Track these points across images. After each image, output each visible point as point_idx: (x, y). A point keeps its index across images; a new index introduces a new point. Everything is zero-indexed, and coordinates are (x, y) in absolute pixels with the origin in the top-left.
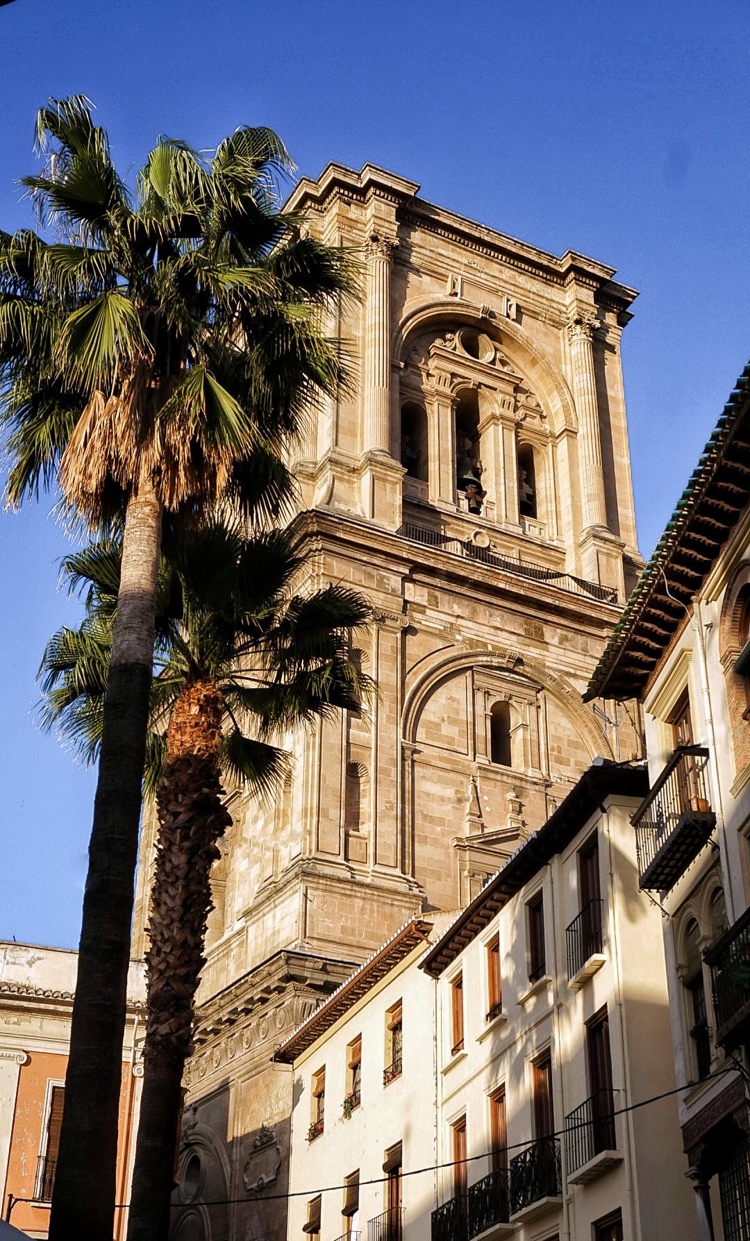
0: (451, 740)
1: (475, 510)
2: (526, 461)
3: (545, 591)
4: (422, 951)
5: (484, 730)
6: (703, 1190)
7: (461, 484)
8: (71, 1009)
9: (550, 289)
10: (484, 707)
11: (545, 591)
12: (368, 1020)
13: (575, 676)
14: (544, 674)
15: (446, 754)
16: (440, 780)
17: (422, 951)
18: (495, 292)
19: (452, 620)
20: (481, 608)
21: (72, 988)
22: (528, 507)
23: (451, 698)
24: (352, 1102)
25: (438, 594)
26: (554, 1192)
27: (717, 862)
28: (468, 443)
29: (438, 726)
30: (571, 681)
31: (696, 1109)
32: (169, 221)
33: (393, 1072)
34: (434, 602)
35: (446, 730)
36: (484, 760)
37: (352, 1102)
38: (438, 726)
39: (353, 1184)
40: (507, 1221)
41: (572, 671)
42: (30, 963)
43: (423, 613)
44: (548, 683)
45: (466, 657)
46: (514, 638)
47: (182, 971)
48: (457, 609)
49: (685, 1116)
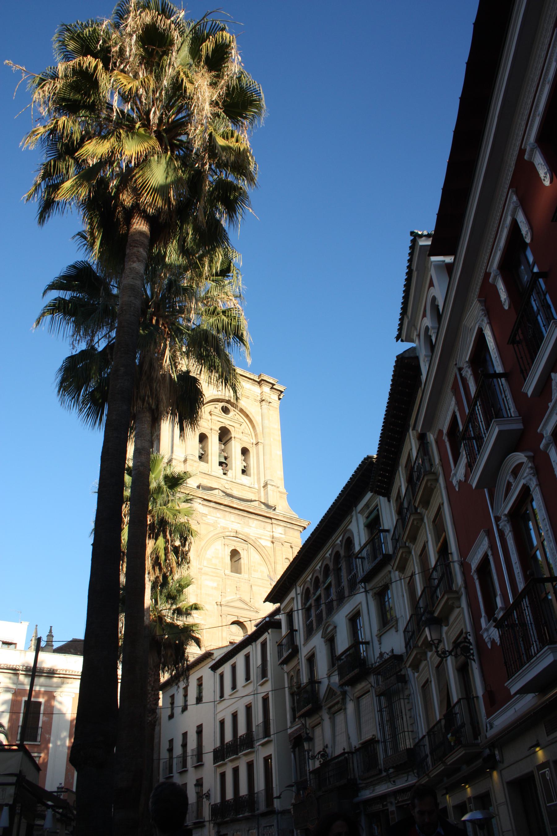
3: (250, 507)
6: (294, 752)
8: (80, 677)
9: (253, 387)
11: (250, 507)
13: (260, 538)
19: (216, 519)
20: (227, 514)
21: (80, 669)
26: (252, 747)
27: (299, 663)
30: (259, 540)
33: (199, 700)
36: (228, 572)
37: (185, 708)
40: (237, 754)
41: (260, 537)
43: (206, 517)
45: (221, 533)
46: (239, 525)
47: (154, 702)
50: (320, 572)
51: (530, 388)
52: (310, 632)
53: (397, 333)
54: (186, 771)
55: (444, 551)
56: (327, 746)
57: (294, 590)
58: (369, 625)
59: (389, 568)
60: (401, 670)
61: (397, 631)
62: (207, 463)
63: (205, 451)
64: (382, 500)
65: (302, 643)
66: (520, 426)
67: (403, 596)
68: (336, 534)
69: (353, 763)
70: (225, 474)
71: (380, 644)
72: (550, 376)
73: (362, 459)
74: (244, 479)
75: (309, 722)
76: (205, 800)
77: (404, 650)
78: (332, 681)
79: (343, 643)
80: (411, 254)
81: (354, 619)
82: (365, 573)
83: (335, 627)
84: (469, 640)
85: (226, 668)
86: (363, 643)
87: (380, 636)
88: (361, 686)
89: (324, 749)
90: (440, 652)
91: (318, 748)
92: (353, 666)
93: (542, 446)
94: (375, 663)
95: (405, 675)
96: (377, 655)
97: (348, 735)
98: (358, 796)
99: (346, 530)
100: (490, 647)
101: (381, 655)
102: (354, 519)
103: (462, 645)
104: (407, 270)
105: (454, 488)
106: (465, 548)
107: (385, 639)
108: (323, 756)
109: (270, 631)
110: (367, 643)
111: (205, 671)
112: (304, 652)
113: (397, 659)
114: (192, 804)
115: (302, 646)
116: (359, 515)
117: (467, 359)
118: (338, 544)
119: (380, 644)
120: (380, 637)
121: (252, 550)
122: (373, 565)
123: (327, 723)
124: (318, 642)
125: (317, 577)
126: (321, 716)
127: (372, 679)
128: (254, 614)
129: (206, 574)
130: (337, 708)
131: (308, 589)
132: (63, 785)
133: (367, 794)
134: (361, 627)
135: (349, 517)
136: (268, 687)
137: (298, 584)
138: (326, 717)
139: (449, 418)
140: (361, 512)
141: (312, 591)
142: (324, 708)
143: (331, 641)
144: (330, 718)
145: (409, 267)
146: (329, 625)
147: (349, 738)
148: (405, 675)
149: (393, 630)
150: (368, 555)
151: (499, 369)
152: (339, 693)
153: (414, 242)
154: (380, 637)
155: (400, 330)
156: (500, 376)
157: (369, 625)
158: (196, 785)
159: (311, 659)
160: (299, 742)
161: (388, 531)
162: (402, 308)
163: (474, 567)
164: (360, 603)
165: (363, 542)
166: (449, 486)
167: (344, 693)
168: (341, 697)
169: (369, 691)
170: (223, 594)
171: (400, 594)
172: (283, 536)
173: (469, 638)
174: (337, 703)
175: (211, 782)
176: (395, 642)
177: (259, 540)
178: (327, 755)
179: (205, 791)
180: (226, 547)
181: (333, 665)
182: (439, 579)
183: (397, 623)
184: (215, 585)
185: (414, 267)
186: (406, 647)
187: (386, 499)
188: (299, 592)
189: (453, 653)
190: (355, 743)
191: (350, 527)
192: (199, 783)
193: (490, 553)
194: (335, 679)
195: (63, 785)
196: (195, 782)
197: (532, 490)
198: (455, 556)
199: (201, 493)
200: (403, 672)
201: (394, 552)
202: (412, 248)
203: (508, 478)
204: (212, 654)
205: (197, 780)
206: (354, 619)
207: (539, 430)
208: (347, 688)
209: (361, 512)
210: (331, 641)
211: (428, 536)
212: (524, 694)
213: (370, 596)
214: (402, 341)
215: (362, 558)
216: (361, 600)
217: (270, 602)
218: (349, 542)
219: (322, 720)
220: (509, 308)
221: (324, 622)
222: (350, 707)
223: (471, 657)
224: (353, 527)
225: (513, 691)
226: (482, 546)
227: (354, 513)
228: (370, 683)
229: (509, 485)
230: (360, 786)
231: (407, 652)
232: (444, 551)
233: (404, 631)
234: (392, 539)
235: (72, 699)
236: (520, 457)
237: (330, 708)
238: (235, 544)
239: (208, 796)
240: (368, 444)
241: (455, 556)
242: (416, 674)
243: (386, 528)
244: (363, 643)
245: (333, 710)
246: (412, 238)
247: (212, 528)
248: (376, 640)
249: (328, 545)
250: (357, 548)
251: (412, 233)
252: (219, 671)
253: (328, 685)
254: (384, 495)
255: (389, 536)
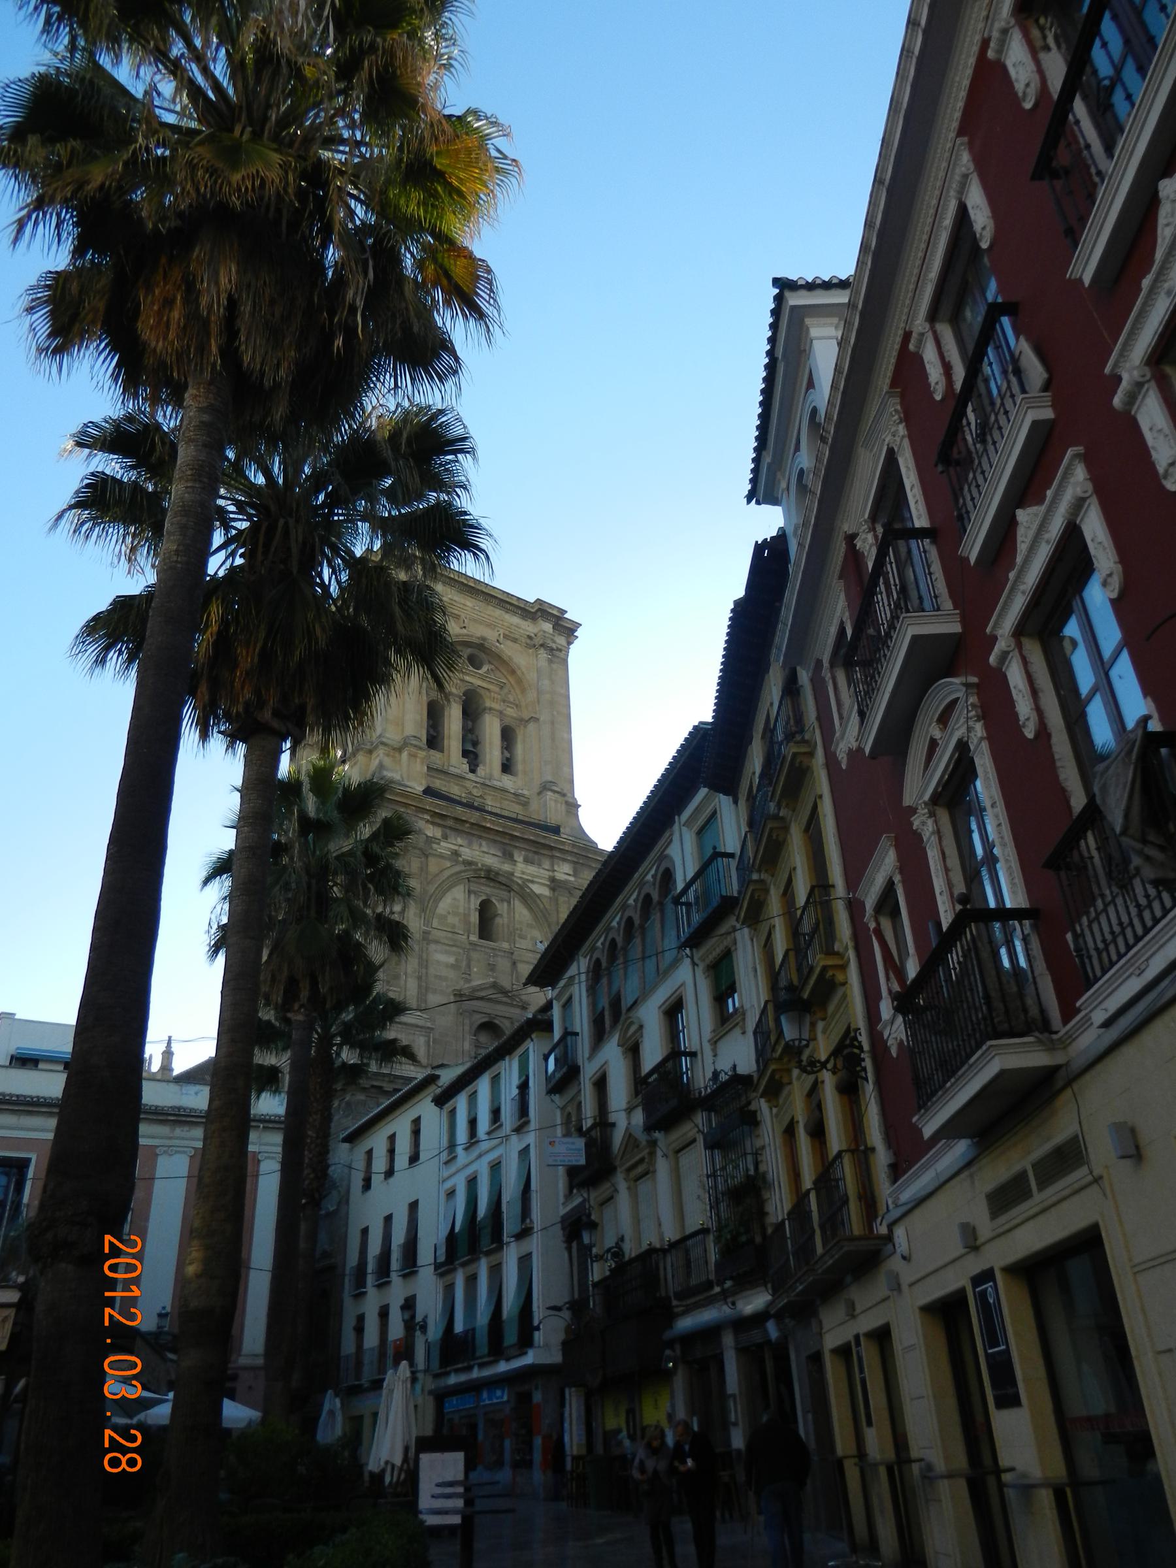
0: (454, 926)
1: (473, 771)
2: (508, 736)
4: (434, 1090)
5: (475, 918)
7: (465, 753)
10: (475, 903)
12: (400, 1125)
13: (532, 882)
14: (513, 881)
15: (450, 935)
16: (447, 952)
17: (434, 1090)
18: (489, 625)
22: (507, 767)
23: (455, 899)
24: (390, 1173)
25: (448, 831)
28: (470, 723)
29: (445, 917)
30: (530, 885)
31: (568, 1208)
32: (384, 1313)
33: (414, 1158)
34: (445, 837)
35: (451, 920)
36: (474, 938)
37: (390, 1173)
38: (445, 917)
39: (388, 1219)
42: (196, 1094)
44: (515, 887)
48: (460, 841)
49: (563, 1211)
50: (618, 930)
51: (973, 548)
52: (599, 1036)
53: (749, 487)
54: (389, 1283)
55: (821, 886)
56: (622, 1239)
57: (575, 964)
58: (698, 1021)
59: (732, 921)
60: (749, 1103)
61: (744, 1033)
62: (442, 751)
63: (438, 732)
64: (724, 802)
65: (587, 1055)
66: (956, 628)
67: (756, 971)
68: (646, 864)
69: (665, 1269)
70: (473, 771)
71: (715, 1056)
72: (1014, 516)
73: (690, 729)
74: (507, 782)
75: (595, 1196)
76: (418, 1333)
77: (754, 1067)
78: (634, 1122)
79: (653, 1053)
80: (774, 327)
81: (673, 1011)
82: (692, 930)
83: (641, 1027)
84: (860, 1043)
85: (461, 1103)
86: (686, 1054)
87: (716, 1042)
88: (687, 1130)
89: (617, 1243)
90: (804, 1063)
91: (610, 1242)
92: (667, 1096)
93: (992, 659)
94: (706, 1088)
95: (755, 1112)
96: (709, 1075)
97: (659, 1218)
98: (671, 1327)
99: (663, 857)
100: (895, 1055)
101: (716, 1074)
102: (676, 837)
103: (846, 1052)
104: (767, 360)
105: (839, 763)
106: (855, 874)
107: (723, 1046)
108: (615, 1255)
109: (533, 1036)
110: (693, 1055)
111: (425, 1108)
112: (589, 1071)
113: (739, 1082)
114: (372, 1349)
115: (586, 1062)
116: (684, 829)
117: (866, 516)
118: (648, 882)
119: (715, 1056)
120: (714, 1043)
121: (518, 905)
122: (705, 915)
123: (623, 1199)
124: (612, 1054)
125: (613, 940)
126: (613, 1185)
127: (700, 1118)
128: (518, 1011)
129: (437, 942)
130: (642, 1172)
131: (598, 962)
132: (168, 1309)
133: (685, 1323)
134: (684, 1027)
135: (667, 834)
136: (531, 1138)
137: (581, 953)
138: (622, 1186)
139: (834, 630)
140: (688, 823)
141: (604, 964)
142: (619, 1170)
143: (633, 1050)
144: (629, 1188)
145: (770, 354)
146: (632, 1023)
147: (660, 1225)
148: (755, 1112)
149: (737, 1031)
150: (697, 898)
151: (920, 519)
152: (644, 1143)
153: (779, 299)
154: (714, 1043)
155: (754, 481)
156: (921, 533)
157: (698, 1021)
158: (403, 1308)
159: (601, 1084)
160: (576, 1227)
161: (732, 855)
162: (757, 438)
163: (870, 903)
164: (683, 984)
165: (690, 874)
166: (831, 761)
167: (653, 1144)
168: (647, 1151)
169: (694, 1141)
170: (467, 975)
171: (750, 965)
172: (572, 879)
173: (860, 1038)
174: (642, 1160)
175: (430, 1304)
176: (740, 1054)
177: (530, 885)
178: (623, 1255)
179: (419, 1318)
180: (472, 896)
181: (637, 1093)
182: (813, 932)
183: (744, 1019)
184: (452, 960)
185: (779, 353)
186: (757, 1062)
187: (731, 798)
188: (583, 970)
189: (829, 1066)
190: (671, 1233)
191: (669, 851)
192: (409, 1305)
193: (897, 879)
194: (639, 1117)
195: (168, 1309)
196: (402, 1302)
197: (972, 748)
198: (840, 889)
199: (430, 803)
200: (753, 1107)
201: (739, 892)
202: (776, 313)
203: (931, 729)
204: (438, 1077)
205: (407, 1300)
206: (673, 1011)
207: (988, 630)
208: (657, 1135)
209: (688, 823)
210: (633, 1050)
211: (797, 856)
212: (954, 1138)
213: (699, 971)
214: (758, 503)
215: (688, 905)
216: (688, 979)
217: (535, 984)
218: (668, 876)
219: (616, 1191)
220: (943, 399)
221: (623, 1018)
222: (662, 1167)
223: (863, 1074)
224: (674, 851)
225: (928, 1131)
226: (886, 865)
227: (676, 827)
228: (697, 1126)
229: (933, 744)
230: (676, 1310)
231: (758, 1070)
232: (821, 886)
233: (755, 1033)
234: (737, 869)
235: (188, 1159)
236: (953, 687)
237: (629, 1170)
238: (488, 890)
239: (424, 1328)
240: (700, 705)
241: (840, 889)
242: (775, 1110)
243: (730, 850)
244: (686, 1054)
245: (633, 1174)
246: (777, 291)
247: (448, 864)
248: (707, 1048)
249: (631, 884)
250: (680, 886)
251: (777, 282)
252: (448, 1106)
253: (627, 1129)
254: (726, 793)
255: (733, 863)
